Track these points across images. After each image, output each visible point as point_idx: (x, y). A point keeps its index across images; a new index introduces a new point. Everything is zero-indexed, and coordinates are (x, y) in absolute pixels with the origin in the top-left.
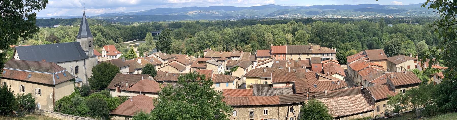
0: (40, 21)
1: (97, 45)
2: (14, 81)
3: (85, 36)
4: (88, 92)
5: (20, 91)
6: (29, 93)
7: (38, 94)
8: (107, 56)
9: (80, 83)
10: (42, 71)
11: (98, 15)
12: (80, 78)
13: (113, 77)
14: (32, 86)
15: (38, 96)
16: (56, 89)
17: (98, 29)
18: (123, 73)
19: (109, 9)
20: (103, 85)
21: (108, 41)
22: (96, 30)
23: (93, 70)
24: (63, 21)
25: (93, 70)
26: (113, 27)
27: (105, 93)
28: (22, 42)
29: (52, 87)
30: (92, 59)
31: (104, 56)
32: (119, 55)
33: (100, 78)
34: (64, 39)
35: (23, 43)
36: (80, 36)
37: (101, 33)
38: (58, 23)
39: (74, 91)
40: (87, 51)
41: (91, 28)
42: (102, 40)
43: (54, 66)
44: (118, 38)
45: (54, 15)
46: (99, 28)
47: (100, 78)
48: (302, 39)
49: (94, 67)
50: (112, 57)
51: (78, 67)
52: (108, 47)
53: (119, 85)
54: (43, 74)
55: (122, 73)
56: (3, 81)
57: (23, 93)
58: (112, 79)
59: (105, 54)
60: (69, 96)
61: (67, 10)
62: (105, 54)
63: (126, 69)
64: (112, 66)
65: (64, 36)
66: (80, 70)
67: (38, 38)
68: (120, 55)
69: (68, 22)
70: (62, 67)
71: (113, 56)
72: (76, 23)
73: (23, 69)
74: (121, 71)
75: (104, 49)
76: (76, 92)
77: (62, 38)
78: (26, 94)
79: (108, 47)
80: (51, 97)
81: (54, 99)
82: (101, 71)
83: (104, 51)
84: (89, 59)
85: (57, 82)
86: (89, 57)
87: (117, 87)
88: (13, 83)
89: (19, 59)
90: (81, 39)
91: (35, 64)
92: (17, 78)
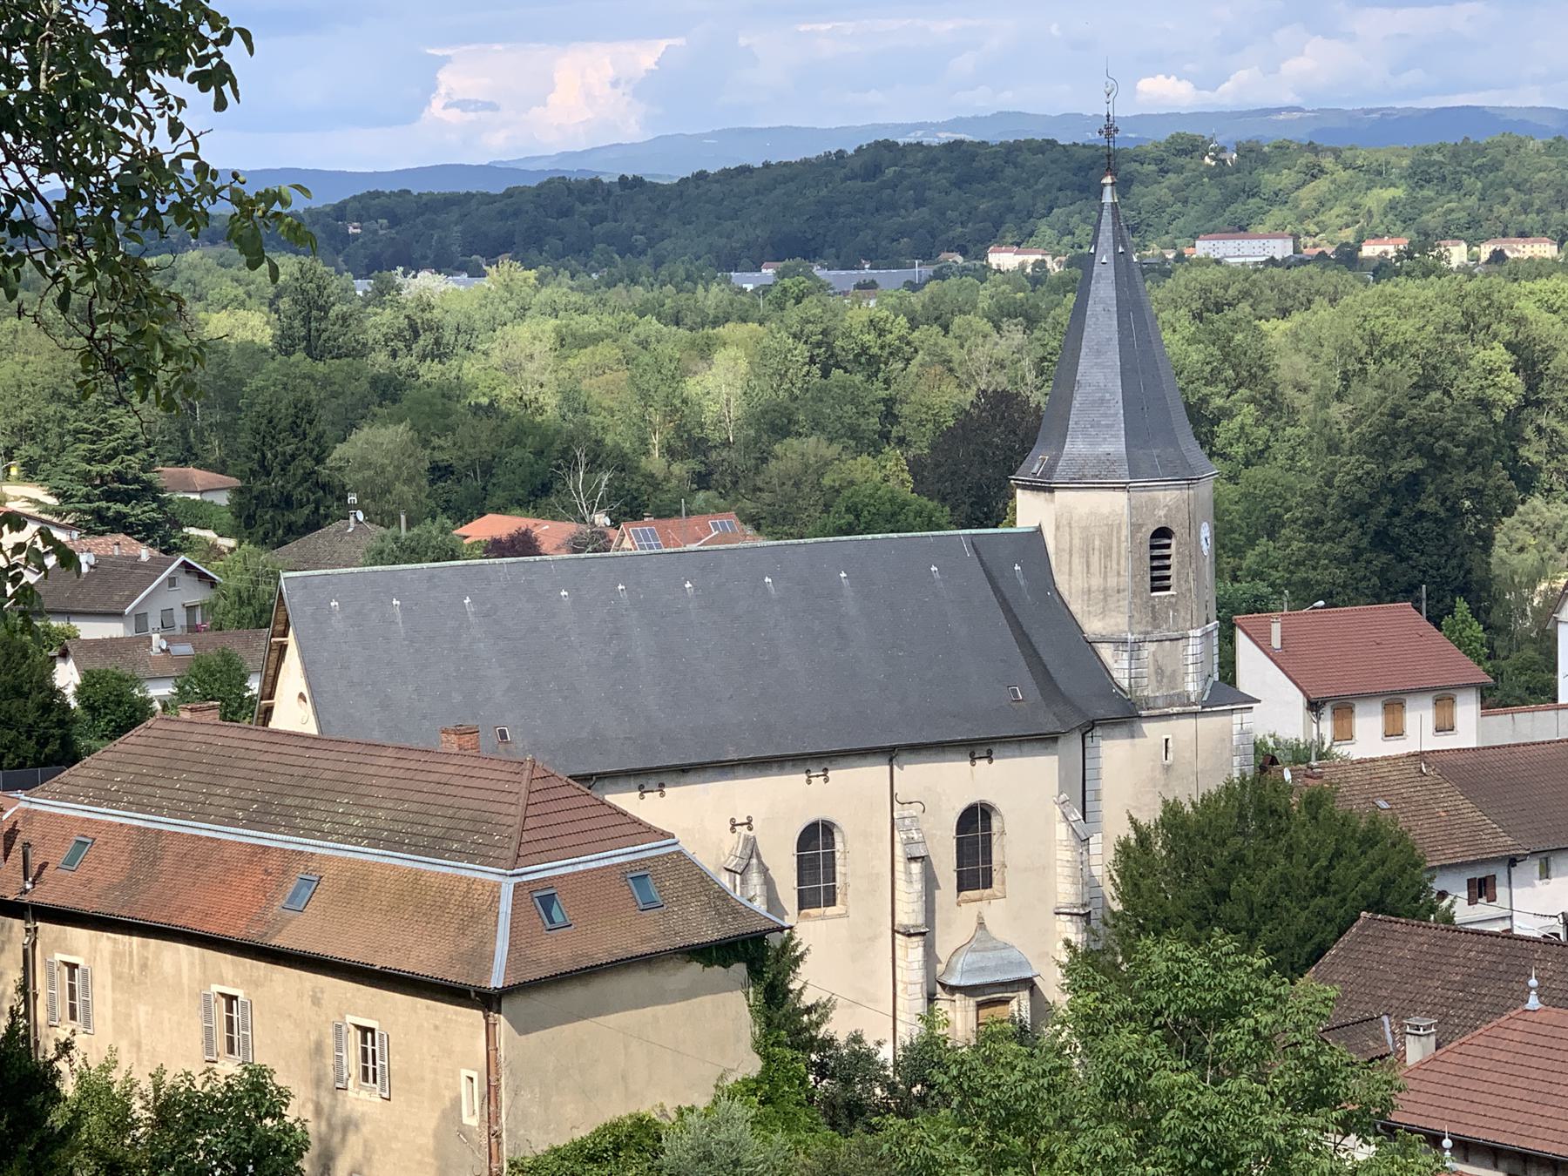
0: (1010, 171)
2: (153, 943)
3: (1108, 462)
5: (209, 1048)
7: (366, 1079)
9: (1006, 1002)
10: (416, 849)
12: (1006, 946)
14: (308, 1002)
15: (360, 1099)
16: (523, 1027)
24: (1322, 185)
29: (480, 1013)
30: (1181, 730)
36: (1050, 469)
38: (1253, 203)
40: (1119, 642)
43: (535, 798)
54: (418, 875)
56: (59, 945)
65: (1204, 400)
66: (1008, 849)
69: (1389, 194)
70: (625, 814)
72: (1504, 211)
73: (251, 824)
80: (472, 1119)
84: (1147, 727)
85: (538, 962)
86: (1148, 703)
88: (144, 966)
90: (1057, 493)
91: (372, 770)
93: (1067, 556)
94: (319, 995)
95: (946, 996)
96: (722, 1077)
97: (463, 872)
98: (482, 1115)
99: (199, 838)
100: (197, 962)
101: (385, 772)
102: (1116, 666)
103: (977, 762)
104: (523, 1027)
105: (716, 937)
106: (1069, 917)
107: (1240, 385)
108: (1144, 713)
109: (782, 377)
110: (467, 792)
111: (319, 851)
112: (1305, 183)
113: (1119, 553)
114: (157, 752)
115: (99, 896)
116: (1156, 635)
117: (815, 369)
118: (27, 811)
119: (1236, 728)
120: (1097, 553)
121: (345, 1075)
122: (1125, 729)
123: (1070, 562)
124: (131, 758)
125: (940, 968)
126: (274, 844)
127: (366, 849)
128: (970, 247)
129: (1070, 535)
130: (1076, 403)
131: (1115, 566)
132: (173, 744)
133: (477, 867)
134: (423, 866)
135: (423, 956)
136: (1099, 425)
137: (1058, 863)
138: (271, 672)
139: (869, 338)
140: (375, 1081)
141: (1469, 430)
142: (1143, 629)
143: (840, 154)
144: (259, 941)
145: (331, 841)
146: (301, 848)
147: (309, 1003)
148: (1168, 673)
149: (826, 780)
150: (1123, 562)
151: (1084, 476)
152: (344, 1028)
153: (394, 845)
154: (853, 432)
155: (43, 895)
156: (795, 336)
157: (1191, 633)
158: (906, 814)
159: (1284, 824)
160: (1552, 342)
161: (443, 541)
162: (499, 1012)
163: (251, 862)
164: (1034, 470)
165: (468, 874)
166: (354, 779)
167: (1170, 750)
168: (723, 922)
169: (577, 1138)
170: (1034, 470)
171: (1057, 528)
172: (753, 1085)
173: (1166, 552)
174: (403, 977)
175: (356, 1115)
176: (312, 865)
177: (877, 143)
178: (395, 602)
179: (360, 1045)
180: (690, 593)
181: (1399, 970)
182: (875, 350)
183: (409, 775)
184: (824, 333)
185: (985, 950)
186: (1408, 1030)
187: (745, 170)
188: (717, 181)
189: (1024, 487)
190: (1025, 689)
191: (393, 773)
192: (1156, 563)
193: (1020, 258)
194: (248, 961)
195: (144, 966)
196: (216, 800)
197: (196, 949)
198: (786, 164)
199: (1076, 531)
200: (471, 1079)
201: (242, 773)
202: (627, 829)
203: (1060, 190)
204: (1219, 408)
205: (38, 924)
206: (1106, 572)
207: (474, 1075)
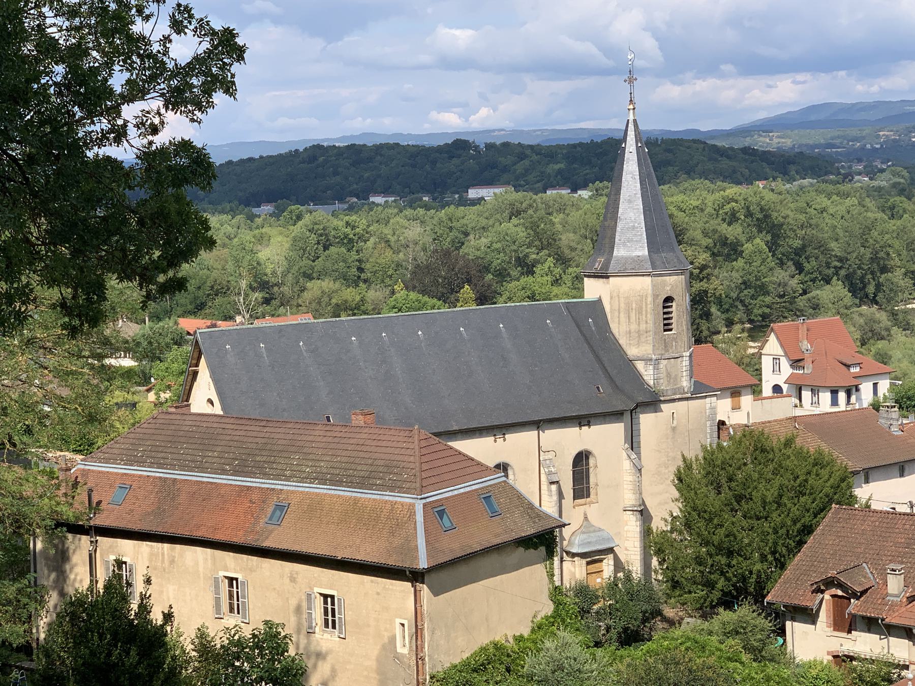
1: (740, 315)
2: (178, 547)
3: (638, 260)
4: (645, 620)
6: (266, 623)
7: (327, 626)
8: (794, 392)
9: (601, 561)
10: (351, 484)
11: (762, 115)
12: (600, 530)
13: (808, 530)
14: (287, 581)
15: (325, 639)
16: (436, 592)
17: (749, 214)
18: (873, 507)
19: (842, 73)
20: (744, 579)
21: (818, 292)
22: (732, 218)
23: (680, 480)
24: (526, 162)
25: (682, 480)
26: (849, 202)
27: (737, 633)
28: (258, 295)
29: (409, 584)
31: (777, 389)
32: (875, 385)
33: (722, 532)
34: (530, 279)
35: (267, 301)
37: (769, 238)
39: (548, 608)
40: (647, 360)
41: (702, 210)
42: (771, 288)
43: (424, 451)
44: (884, 270)
45: (472, 117)
46: (754, 208)
47: (722, 532)
48: (47, 328)
49: (685, 460)
50: (826, 397)
51: (587, 458)
52: (803, 332)
53: (840, 586)
54: (356, 500)
55: (868, 506)
56: (111, 549)
57: (231, 621)
58: (801, 543)
59: (780, 380)
60: (519, 639)
61: (562, 86)
62: (780, 380)
63: (872, 485)
64: (801, 455)
65: (526, 256)
66: (597, 476)
67: (361, 270)
68: (884, 385)
70: (472, 460)
71: (834, 392)
73: (236, 473)
74: (862, 492)
75: (773, 346)
76: (557, 618)
77: (514, 273)
78: (247, 632)
79: (803, 332)
80: (403, 649)
81: (420, 659)
82: (733, 484)
83: (776, 359)
84: (663, 406)
87: (827, 596)
88: (172, 562)
89: (218, 410)
90: (611, 279)
91: (311, 438)
92: (198, 527)
93: (617, 314)
94: (295, 576)
95: (569, 559)
96: (535, 616)
97: (387, 498)
98: (410, 647)
99: (202, 482)
100: (209, 558)
101: (319, 439)
102: (646, 373)
103: (583, 428)
104: (436, 592)
105: (532, 531)
106: (631, 512)
107: (542, 249)
108: (662, 398)
109: (304, 251)
110: (379, 450)
111: (285, 488)
112: (519, 162)
113: (646, 311)
114: (163, 432)
115: (140, 520)
116: (667, 356)
117: (321, 247)
118: (83, 470)
119: (708, 406)
120: (634, 311)
121: (314, 624)
122: (652, 407)
123: (619, 317)
124: (147, 437)
125: (565, 543)
126: (254, 485)
127: (318, 486)
128: (361, 195)
129: (619, 301)
130: (618, 229)
131: (644, 317)
132: (173, 427)
133: (397, 494)
134: (359, 495)
135: (368, 550)
136: (632, 240)
137: (625, 482)
138: (188, 388)
139: (348, 230)
140: (238, 613)
141: (700, 261)
142: (660, 352)
143: (296, 151)
144: (255, 544)
145: (294, 482)
146: (273, 486)
147: (288, 580)
148: (673, 376)
149: (505, 440)
150: (648, 315)
151: (626, 269)
152: (313, 596)
153: (336, 482)
154: (345, 278)
155: (100, 520)
156: (310, 231)
157: (684, 354)
158: (546, 457)
159: (771, 456)
160: (684, 226)
161: (176, 329)
162: (423, 583)
163: (239, 496)
164: (596, 267)
165: (391, 498)
166: (299, 444)
167: (675, 419)
168: (534, 522)
169: (465, 658)
170: (596, 267)
171: (611, 298)
172: (552, 620)
173: (669, 310)
174: (355, 563)
175: (324, 650)
176: (282, 497)
177: (314, 145)
178: (261, 345)
179: (322, 605)
180: (422, 337)
181: (865, 536)
182: (351, 236)
183: (336, 440)
184: (324, 229)
185: (590, 532)
186: (889, 571)
187: (251, 160)
188: (238, 165)
189: (589, 276)
190: (604, 388)
191: (325, 439)
192: (665, 316)
193: (385, 199)
194: (255, 558)
195: (172, 562)
196: (210, 460)
197: (209, 550)
198: (271, 157)
199: (622, 300)
200: (403, 625)
201: (223, 443)
202: (476, 469)
203: (402, 166)
204: (534, 259)
205: (98, 538)
206: (639, 322)
207: (406, 622)
